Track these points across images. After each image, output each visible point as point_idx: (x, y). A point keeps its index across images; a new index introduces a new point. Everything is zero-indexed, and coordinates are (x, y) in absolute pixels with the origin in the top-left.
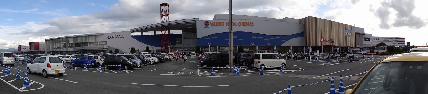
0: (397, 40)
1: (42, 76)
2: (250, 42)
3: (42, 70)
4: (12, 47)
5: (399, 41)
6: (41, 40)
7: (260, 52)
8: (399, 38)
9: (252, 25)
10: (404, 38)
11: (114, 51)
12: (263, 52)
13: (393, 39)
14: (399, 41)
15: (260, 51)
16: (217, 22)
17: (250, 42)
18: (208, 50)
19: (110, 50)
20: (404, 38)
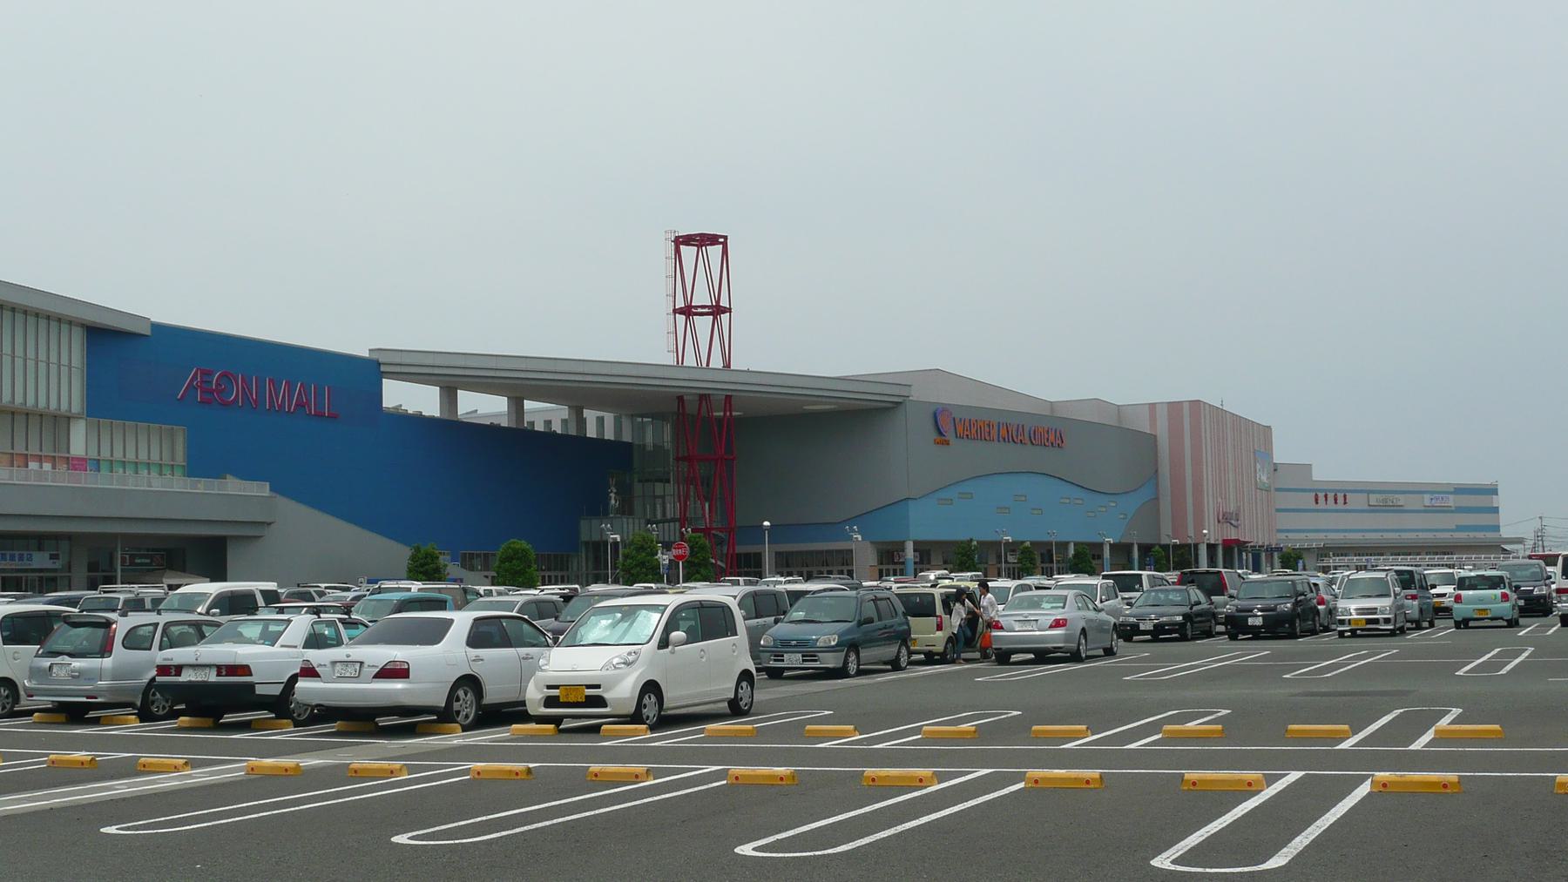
0: (1452, 501)
1: (556, 630)
2: (766, 523)
3: (743, 668)
4: (1091, 577)
5: (1459, 510)
6: (1555, 615)
7: (553, 581)
8: (1460, 490)
9: (598, 687)
10: (1493, 491)
11: (477, 563)
12: (891, 572)
13: (1427, 497)
14: (1459, 510)
15: (898, 571)
16: (353, 609)
17: (766, 523)
18: (1014, 571)
19: (889, 538)
20: (1493, 491)
